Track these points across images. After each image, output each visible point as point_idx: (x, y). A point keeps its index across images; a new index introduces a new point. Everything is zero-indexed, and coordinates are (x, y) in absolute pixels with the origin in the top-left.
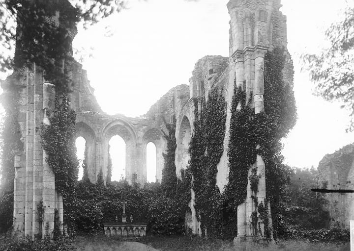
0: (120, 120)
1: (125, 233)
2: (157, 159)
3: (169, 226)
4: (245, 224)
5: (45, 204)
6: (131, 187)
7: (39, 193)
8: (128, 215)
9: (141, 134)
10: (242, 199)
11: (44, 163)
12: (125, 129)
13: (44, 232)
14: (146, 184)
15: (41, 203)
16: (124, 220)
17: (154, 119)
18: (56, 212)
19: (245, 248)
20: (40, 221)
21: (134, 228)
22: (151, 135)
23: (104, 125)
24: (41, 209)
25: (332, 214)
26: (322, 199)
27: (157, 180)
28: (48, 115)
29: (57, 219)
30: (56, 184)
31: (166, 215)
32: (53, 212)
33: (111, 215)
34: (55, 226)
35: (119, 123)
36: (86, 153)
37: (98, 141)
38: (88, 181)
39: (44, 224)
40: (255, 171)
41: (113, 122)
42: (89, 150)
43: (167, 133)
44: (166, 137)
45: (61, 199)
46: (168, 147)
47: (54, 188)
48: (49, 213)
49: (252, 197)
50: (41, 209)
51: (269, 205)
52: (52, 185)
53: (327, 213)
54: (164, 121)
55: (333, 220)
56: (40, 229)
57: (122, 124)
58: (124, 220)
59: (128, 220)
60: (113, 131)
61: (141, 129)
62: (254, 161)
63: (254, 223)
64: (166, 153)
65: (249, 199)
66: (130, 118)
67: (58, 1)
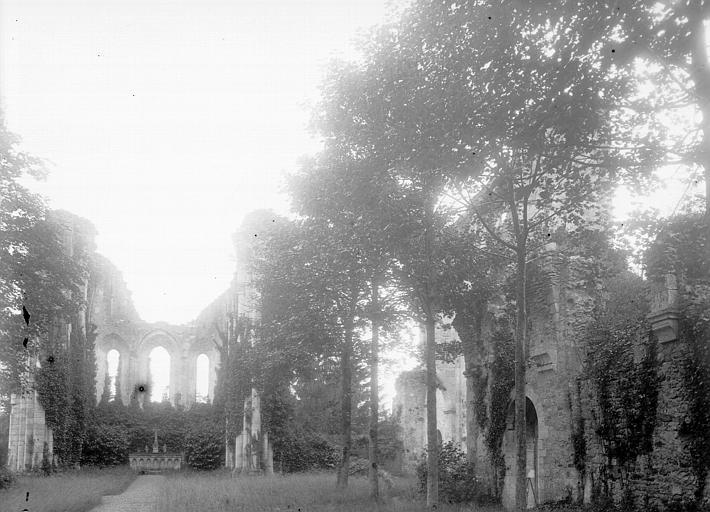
0: (160, 329)
1: (156, 466)
2: (210, 374)
3: (208, 457)
4: (241, 455)
5: (35, 437)
6: (173, 410)
7: (31, 427)
8: (161, 445)
9: (187, 345)
10: (239, 431)
11: (36, 401)
12: (168, 338)
13: (33, 463)
14: (195, 405)
15: (32, 436)
16: (156, 450)
17: (204, 327)
18: (46, 444)
19: (570, 493)
20: (31, 452)
21: (166, 459)
22: (199, 345)
23: (141, 336)
24: (31, 442)
25: (406, 445)
26: (397, 426)
27: (209, 401)
28: (40, 359)
29: (46, 451)
30: (47, 419)
31: (203, 445)
32: (43, 444)
33: (140, 443)
34: (44, 457)
35: (159, 333)
36: (119, 370)
37: (133, 354)
38: (120, 402)
39: (34, 456)
40: (250, 403)
41: (157, 330)
42: (123, 365)
43: (221, 343)
44: (219, 348)
45: (51, 432)
46: (222, 360)
47: (44, 422)
48: (38, 445)
49: (247, 429)
50: (31, 442)
51: (266, 436)
52: (42, 421)
53: (401, 443)
54: (217, 328)
55: (408, 451)
56: (31, 460)
57: (164, 334)
58: (156, 450)
59: (161, 450)
60: (154, 342)
61: (187, 340)
62: (249, 394)
63: (248, 455)
64: (219, 367)
65: (245, 432)
66: (174, 327)
67: (3, 333)
